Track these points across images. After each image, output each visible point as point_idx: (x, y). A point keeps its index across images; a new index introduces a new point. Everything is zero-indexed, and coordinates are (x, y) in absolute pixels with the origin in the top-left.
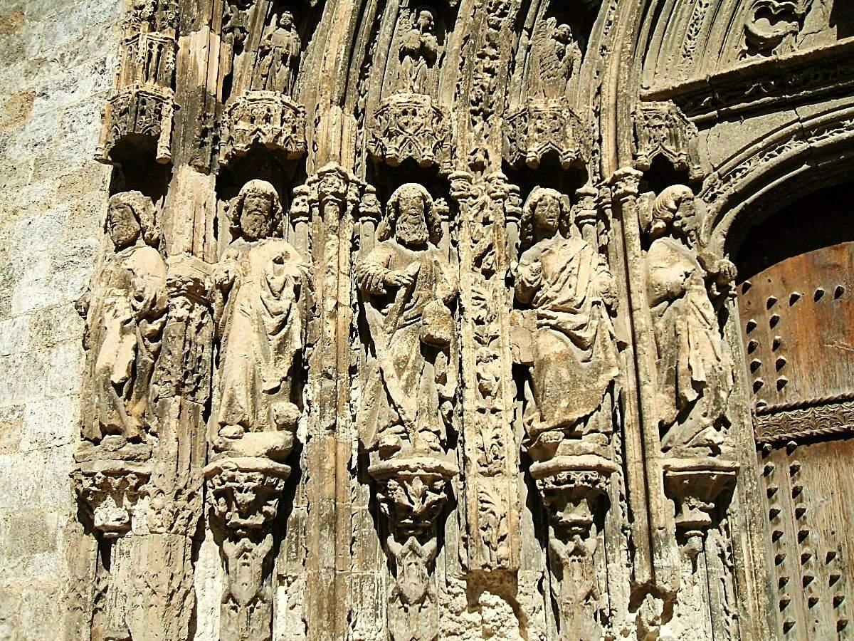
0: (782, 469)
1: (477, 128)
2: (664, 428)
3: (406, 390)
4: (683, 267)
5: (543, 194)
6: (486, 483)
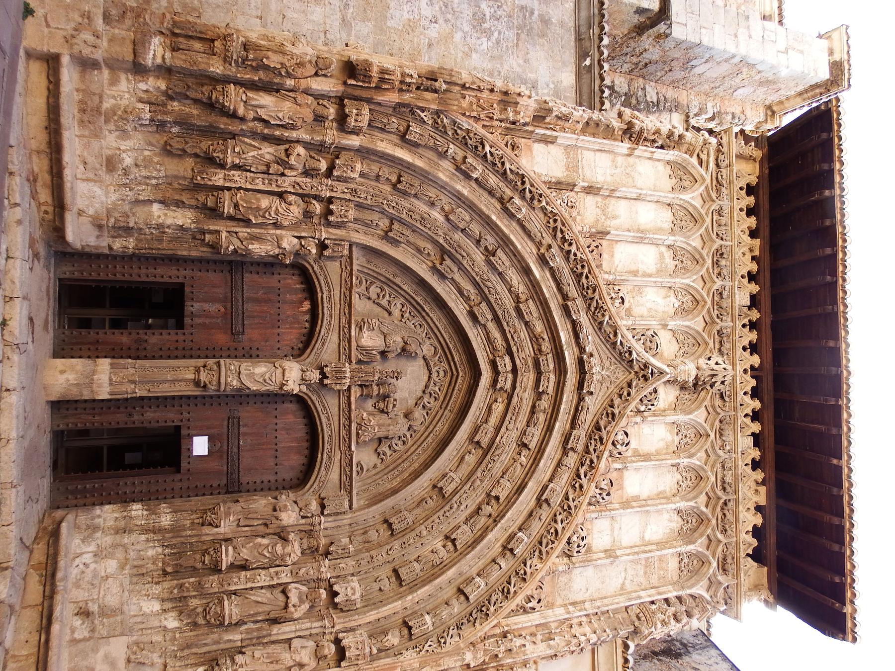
0: (403, 584)
2: (236, 233)
3: (253, 156)
4: (288, 247)
5: (318, 208)
6: (222, 176)
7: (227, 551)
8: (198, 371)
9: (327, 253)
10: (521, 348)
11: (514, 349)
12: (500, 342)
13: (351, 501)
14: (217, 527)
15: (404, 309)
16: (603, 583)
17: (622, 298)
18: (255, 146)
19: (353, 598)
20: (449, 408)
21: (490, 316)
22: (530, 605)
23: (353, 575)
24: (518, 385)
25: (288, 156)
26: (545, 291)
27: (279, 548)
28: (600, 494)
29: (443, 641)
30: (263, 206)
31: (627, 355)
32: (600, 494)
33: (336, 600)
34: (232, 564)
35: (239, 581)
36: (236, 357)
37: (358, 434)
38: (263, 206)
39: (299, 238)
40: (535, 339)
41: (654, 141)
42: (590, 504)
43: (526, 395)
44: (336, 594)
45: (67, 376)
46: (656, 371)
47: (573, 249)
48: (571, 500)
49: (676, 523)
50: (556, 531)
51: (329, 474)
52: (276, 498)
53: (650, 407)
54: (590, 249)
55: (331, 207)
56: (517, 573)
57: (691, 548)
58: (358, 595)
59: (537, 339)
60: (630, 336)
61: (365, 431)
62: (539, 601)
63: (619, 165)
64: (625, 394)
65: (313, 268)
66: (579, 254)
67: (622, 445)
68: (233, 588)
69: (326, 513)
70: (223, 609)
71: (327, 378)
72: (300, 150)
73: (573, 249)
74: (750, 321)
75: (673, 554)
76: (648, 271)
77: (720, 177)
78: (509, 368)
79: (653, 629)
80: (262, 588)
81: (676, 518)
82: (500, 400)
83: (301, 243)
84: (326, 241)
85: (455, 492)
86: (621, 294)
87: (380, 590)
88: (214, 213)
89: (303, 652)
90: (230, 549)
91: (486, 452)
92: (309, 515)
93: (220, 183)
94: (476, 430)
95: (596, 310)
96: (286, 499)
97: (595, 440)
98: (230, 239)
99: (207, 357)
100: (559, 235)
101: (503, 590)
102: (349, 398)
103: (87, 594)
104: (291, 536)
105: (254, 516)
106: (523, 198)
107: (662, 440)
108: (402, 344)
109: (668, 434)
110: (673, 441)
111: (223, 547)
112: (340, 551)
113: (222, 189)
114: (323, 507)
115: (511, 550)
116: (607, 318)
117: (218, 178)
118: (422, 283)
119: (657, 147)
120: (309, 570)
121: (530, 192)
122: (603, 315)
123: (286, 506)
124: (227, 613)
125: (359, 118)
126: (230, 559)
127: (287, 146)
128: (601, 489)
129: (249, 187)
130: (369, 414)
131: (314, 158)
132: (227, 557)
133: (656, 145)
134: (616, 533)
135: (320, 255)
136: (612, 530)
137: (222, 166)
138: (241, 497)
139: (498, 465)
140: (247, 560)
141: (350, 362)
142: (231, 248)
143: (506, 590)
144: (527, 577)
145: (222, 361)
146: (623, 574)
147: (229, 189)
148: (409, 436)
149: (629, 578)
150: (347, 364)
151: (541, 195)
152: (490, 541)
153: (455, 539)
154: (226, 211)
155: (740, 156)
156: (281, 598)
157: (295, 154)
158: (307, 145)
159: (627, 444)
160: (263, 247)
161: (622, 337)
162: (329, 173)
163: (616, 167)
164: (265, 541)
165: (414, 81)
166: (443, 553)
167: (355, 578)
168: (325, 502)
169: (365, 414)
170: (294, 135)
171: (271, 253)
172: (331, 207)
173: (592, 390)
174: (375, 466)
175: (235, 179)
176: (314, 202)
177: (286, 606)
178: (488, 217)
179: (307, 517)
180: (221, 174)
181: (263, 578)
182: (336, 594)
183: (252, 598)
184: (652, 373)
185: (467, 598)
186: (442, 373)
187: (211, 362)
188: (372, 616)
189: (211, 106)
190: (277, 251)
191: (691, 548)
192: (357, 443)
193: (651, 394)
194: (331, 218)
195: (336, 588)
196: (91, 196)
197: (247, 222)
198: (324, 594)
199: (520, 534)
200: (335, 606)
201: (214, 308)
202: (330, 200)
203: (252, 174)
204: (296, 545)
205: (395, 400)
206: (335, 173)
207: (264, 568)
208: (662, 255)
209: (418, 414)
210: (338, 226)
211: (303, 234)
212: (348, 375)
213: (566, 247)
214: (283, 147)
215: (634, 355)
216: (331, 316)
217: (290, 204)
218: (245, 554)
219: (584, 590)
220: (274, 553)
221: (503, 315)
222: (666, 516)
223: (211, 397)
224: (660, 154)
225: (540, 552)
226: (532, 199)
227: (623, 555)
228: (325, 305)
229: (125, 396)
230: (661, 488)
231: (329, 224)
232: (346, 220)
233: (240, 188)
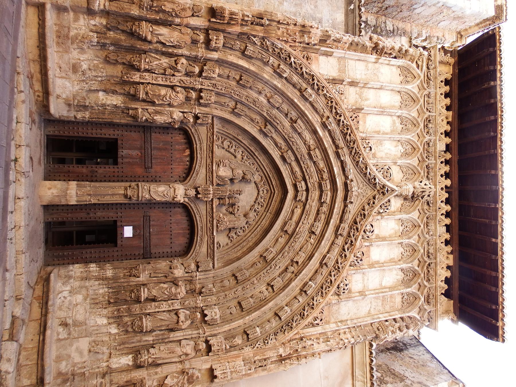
0: (244, 310)
1: (210, 85)
2: (147, 109)
4: (176, 118)
5: (194, 95)
6: (138, 76)
7: (144, 291)
8: (126, 189)
9: (199, 121)
10: (311, 177)
11: (307, 177)
12: (299, 173)
13: (213, 264)
14: (138, 277)
15: (243, 155)
16: (358, 310)
17: (370, 147)
18: (157, 59)
19: (215, 318)
20: (269, 211)
21: (293, 158)
22: (316, 322)
23: (215, 305)
24: (309, 198)
25: (176, 64)
26: (325, 143)
27: (173, 290)
28: (357, 260)
29: (266, 342)
30: (162, 94)
31: (373, 180)
32: (357, 260)
33: (206, 319)
34: (147, 298)
35: (151, 308)
36: (148, 181)
37: (217, 226)
38: (162, 94)
39: (183, 112)
40: (319, 172)
41: (390, 54)
42: (350, 266)
43: (314, 204)
44: (206, 315)
45: (52, 191)
46: (389, 189)
47: (342, 118)
48: (340, 263)
49: (400, 276)
50: (331, 281)
51: (201, 249)
52: (171, 262)
53: (386, 210)
54: (352, 119)
55: (202, 94)
56: (309, 305)
57: (409, 290)
58: (218, 316)
59: (320, 172)
60: (375, 169)
61: (221, 224)
62: (321, 320)
63: (369, 68)
64: (372, 203)
65: (191, 130)
66: (345, 122)
67: (369, 232)
68: (148, 311)
69: (199, 270)
70: (142, 323)
71: (200, 194)
72: (183, 60)
73: (342, 118)
74: (445, 159)
75: (398, 294)
76: (386, 131)
77: (429, 75)
78: (304, 188)
79: (387, 335)
80: (164, 311)
81: (400, 273)
82: (299, 206)
83: (184, 116)
84: (199, 115)
85: (273, 259)
86: (370, 145)
87: (231, 313)
88: (134, 97)
89: (188, 347)
90: (146, 289)
91: (291, 236)
92: (190, 271)
93: (138, 80)
94: (285, 224)
95: (355, 155)
96: (177, 262)
97: (354, 229)
98: (144, 113)
99: (131, 181)
100: (334, 111)
101: (301, 314)
102: (212, 205)
103: (65, 314)
104: (180, 283)
105: (159, 271)
106: (313, 89)
107: (393, 229)
108: (242, 174)
109: (397, 226)
110: (399, 229)
111: (142, 289)
112: (208, 292)
113: (139, 83)
114: (198, 267)
115: (305, 292)
116: (361, 159)
117: (136, 77)
118: (254, 139)
119: (392, 58)
120: (190, 302)
121: (317, 85)
122: (359, 157)
123: (177, 266)
124: (145, 325)
125: (218, 42)
126: (146, 296)
127: (176, 58)
128: (357, 257)
129: (154, 82)
130: (224, 214)
131: (191, 65)
132: (144, 294)
133: (392, 56)
134: (366, 281)
135: (195, 123)
136: (363, 280)
137: (139, 70)
138: (152, 261)
139: (298, 244)
140: (155, 296)
141: (213, 185)
142: (144, 118)
143: (302, 314)
144: (315, 307)
145: (140, 184)
146: (369, 305)
147: (143, 83)
148: (246, 227)
149: (373, 307)
150: (211, 186)
151: (323, 87)
152: (293, 287)
153: (273, 285)
154: (141, 97)
155: (441, 62)
156: (175, 317)
157: (180, 63)
158: (188, 58)
159: (373, 232)
160: (162, 118)
161: (370, 170)
162: (200, 75)
163: (368, 70)
164: (165, 286)
165: (250, 19)
166: (266, 293)
167: (216, 307)
168: (199, 264)
169: (221, 215)
170: (180, 51)
171: (167, 121)
172: (202, 94)
173: (352, 201)
174: (227, 244)
175: (146, 77)
176: (192, 91)
177: (178, 322)
178: (292, 100)
179: (189, 272)
180: (138, 74)
181: (165, 306)
182: (206, 315)
183: (159, 317)
184: (387, 191)
185: (280, 318)
186: (265, 192)
187: (133, 184)
188: (226, 328)
189: (132, 34)
190: (170, 120)
191: (409, 290)
192: (217, 231)
193: (386, 203)
194: (201, 101)
195: (206, 312)
196: (64, 88)
197: (153, 103)
198: (199, 315)
199: (310, 283)
200: (205, 322)
201: (135, 153)
202: (201, 90)
203: (156, 75)
204: (183, 288)
205: (239, 207)
206: (204, 75)
207: (165, 301)
208: (394, 122)
209: (252, 215)
210: (206, 106)
211: (186, 110)
212: (212, 192)
213: (338, 118)
214: (173, 59)
215: (377, 180)
216: (201, 158)
217: (178, 93)
218: (154, 292)
219: (347, 314)
220: (170, 292)
221: (301, 158)
222: (395, 272)
223: (134, 204)
224: (394, 61)
225: (322, 292)
226: (318, 89)
227: (369, 294)
228: (198, 152)
229: (85, 203)
230: (392, 257)
231: (200, 105)
232: (210, 102)
233: (149, 83)
